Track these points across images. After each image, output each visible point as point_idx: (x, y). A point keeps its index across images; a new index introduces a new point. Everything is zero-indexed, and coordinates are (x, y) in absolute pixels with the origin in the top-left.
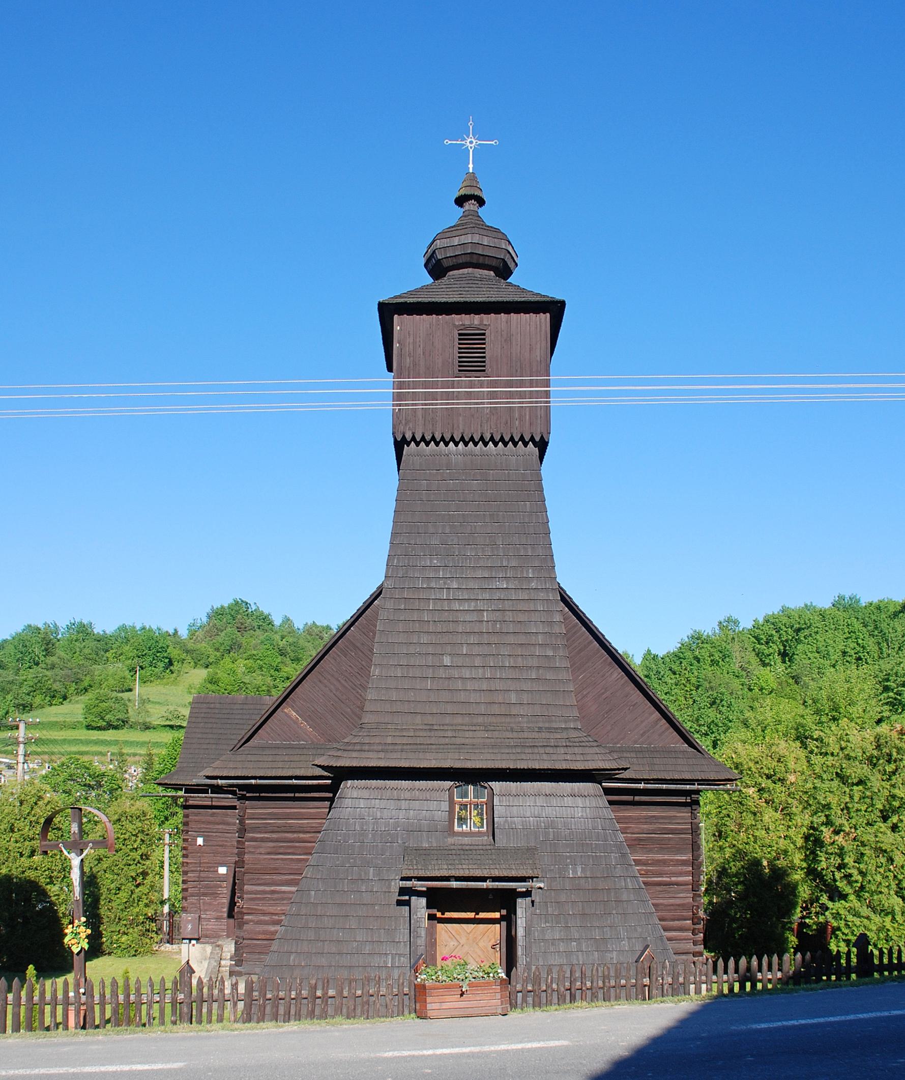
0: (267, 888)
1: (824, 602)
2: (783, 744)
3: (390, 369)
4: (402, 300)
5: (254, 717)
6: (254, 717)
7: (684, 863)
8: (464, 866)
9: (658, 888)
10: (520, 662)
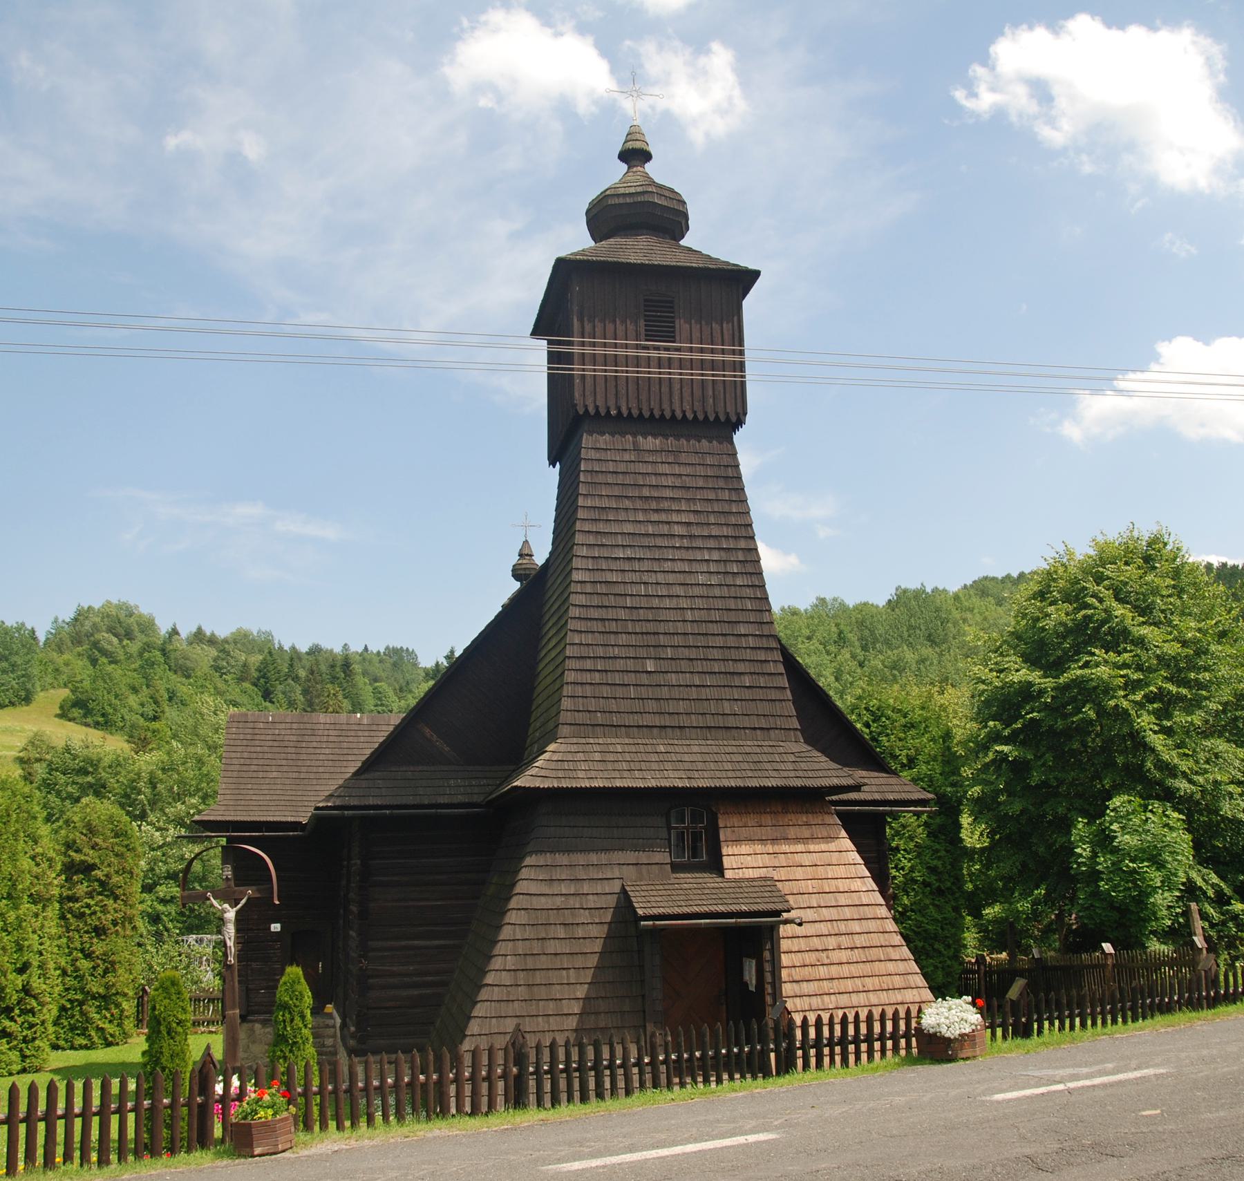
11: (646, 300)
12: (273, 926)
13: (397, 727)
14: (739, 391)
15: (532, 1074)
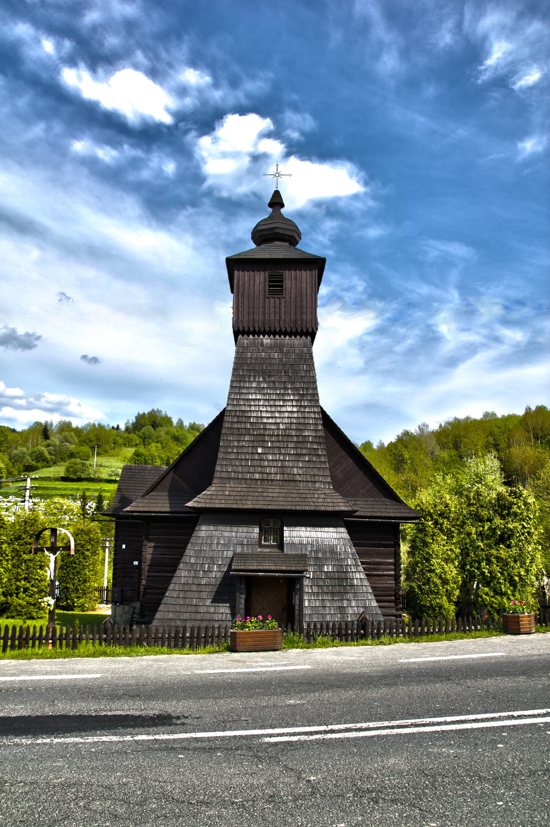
0: (159, 574)
1: (477, 415)
2: (448, 497)
3: (232, 292)
4: (239, 257)
5: (147, 486)
6: (147, 486)
7: (390, 564)
8: (266, 564)
9: (377, 578)
10: (299, 451)
11: (269, 275)
12: (134, 562)
13: (381, 478)
14: (316, 324)
15: (181, 638)
